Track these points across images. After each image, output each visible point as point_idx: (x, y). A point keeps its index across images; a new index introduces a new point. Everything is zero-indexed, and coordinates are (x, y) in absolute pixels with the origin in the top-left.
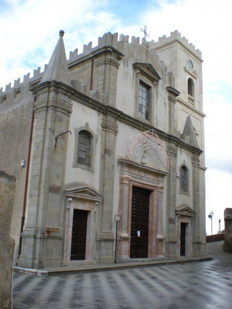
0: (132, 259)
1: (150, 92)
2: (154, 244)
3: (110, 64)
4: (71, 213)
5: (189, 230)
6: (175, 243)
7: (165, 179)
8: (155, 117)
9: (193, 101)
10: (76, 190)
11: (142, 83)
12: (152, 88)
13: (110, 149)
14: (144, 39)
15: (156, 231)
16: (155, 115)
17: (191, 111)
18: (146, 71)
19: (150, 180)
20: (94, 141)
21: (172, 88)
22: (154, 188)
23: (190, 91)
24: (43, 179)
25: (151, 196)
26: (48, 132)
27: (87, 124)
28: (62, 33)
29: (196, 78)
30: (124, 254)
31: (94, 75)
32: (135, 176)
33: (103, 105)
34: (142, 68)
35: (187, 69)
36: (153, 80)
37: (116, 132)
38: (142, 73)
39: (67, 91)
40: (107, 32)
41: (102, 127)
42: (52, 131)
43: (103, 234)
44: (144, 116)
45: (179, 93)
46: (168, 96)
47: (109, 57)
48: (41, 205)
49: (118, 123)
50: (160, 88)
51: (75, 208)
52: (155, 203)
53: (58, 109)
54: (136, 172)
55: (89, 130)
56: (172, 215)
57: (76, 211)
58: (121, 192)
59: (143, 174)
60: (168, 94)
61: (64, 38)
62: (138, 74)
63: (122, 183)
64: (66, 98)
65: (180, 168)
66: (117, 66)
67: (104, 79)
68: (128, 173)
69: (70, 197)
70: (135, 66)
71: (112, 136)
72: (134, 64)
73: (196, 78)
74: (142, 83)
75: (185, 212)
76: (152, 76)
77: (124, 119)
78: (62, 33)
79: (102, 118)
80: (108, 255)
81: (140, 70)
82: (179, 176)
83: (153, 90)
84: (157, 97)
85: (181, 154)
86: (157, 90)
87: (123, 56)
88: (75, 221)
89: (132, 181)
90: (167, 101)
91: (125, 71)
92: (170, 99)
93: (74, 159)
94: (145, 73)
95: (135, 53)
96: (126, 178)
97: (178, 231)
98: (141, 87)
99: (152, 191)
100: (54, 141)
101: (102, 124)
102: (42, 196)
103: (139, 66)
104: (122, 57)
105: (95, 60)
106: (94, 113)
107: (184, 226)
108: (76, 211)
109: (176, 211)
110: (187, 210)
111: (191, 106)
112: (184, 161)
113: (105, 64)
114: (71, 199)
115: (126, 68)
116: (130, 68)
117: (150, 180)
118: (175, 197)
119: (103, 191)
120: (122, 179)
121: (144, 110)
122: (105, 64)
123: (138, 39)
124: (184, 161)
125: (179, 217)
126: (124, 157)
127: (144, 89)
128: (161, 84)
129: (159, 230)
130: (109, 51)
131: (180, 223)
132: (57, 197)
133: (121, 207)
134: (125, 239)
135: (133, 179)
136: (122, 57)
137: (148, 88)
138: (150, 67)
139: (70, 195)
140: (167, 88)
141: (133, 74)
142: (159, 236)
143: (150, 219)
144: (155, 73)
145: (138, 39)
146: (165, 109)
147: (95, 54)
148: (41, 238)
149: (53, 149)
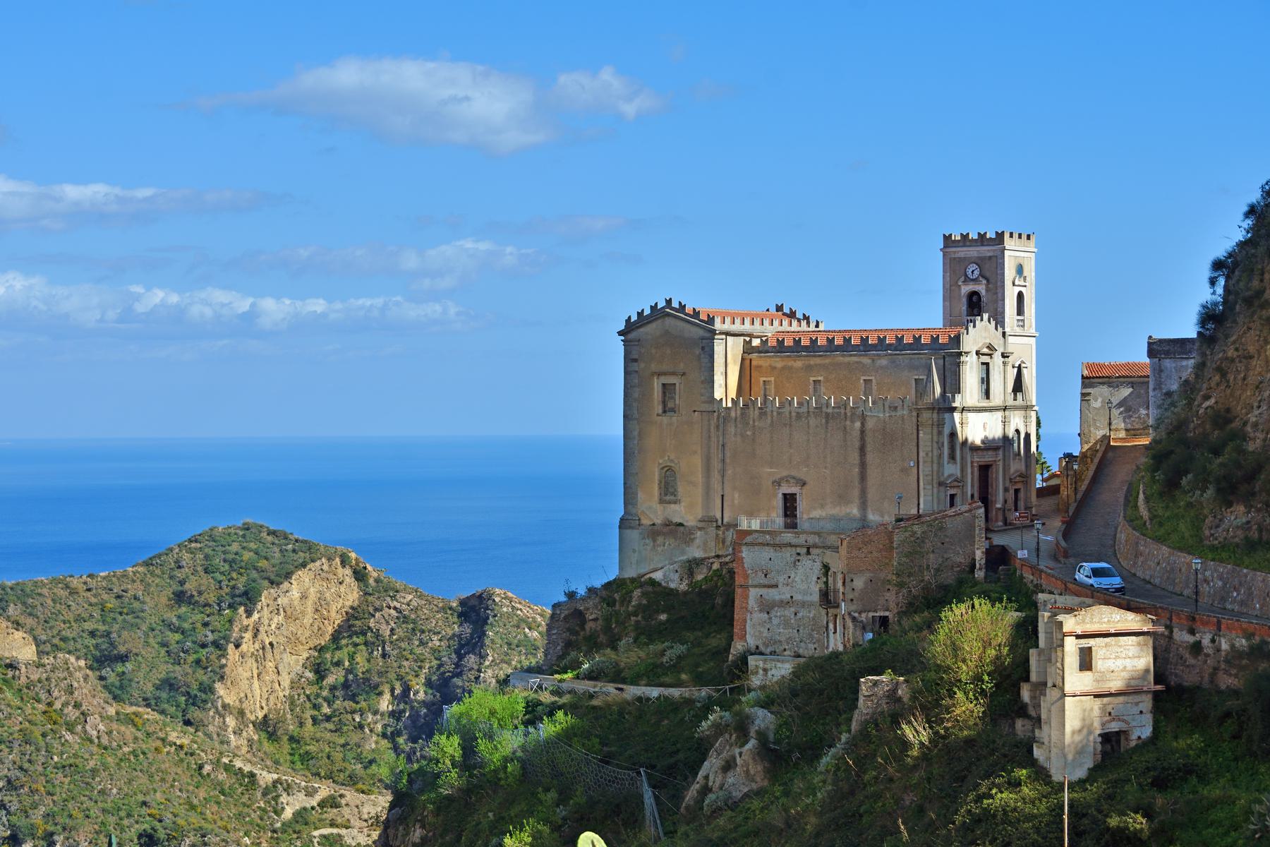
2: (994, 512)
5: (1022, 495)
15: (995, 501)
17: (674, 320)
23: (636, 393)
24: (935, 477)
26: (935, 445)
31: (946, 373)
42: (937, 443)
48: (935, 496)
52: (994, 476)
58: (972, 473)
63: (972, 466)
66: (1147, 457)
102: (935, 490)
107: (1017, 491)
118: (1009, 465)
120: (972, 462)
133: (972, 486)
143: (990, 490)
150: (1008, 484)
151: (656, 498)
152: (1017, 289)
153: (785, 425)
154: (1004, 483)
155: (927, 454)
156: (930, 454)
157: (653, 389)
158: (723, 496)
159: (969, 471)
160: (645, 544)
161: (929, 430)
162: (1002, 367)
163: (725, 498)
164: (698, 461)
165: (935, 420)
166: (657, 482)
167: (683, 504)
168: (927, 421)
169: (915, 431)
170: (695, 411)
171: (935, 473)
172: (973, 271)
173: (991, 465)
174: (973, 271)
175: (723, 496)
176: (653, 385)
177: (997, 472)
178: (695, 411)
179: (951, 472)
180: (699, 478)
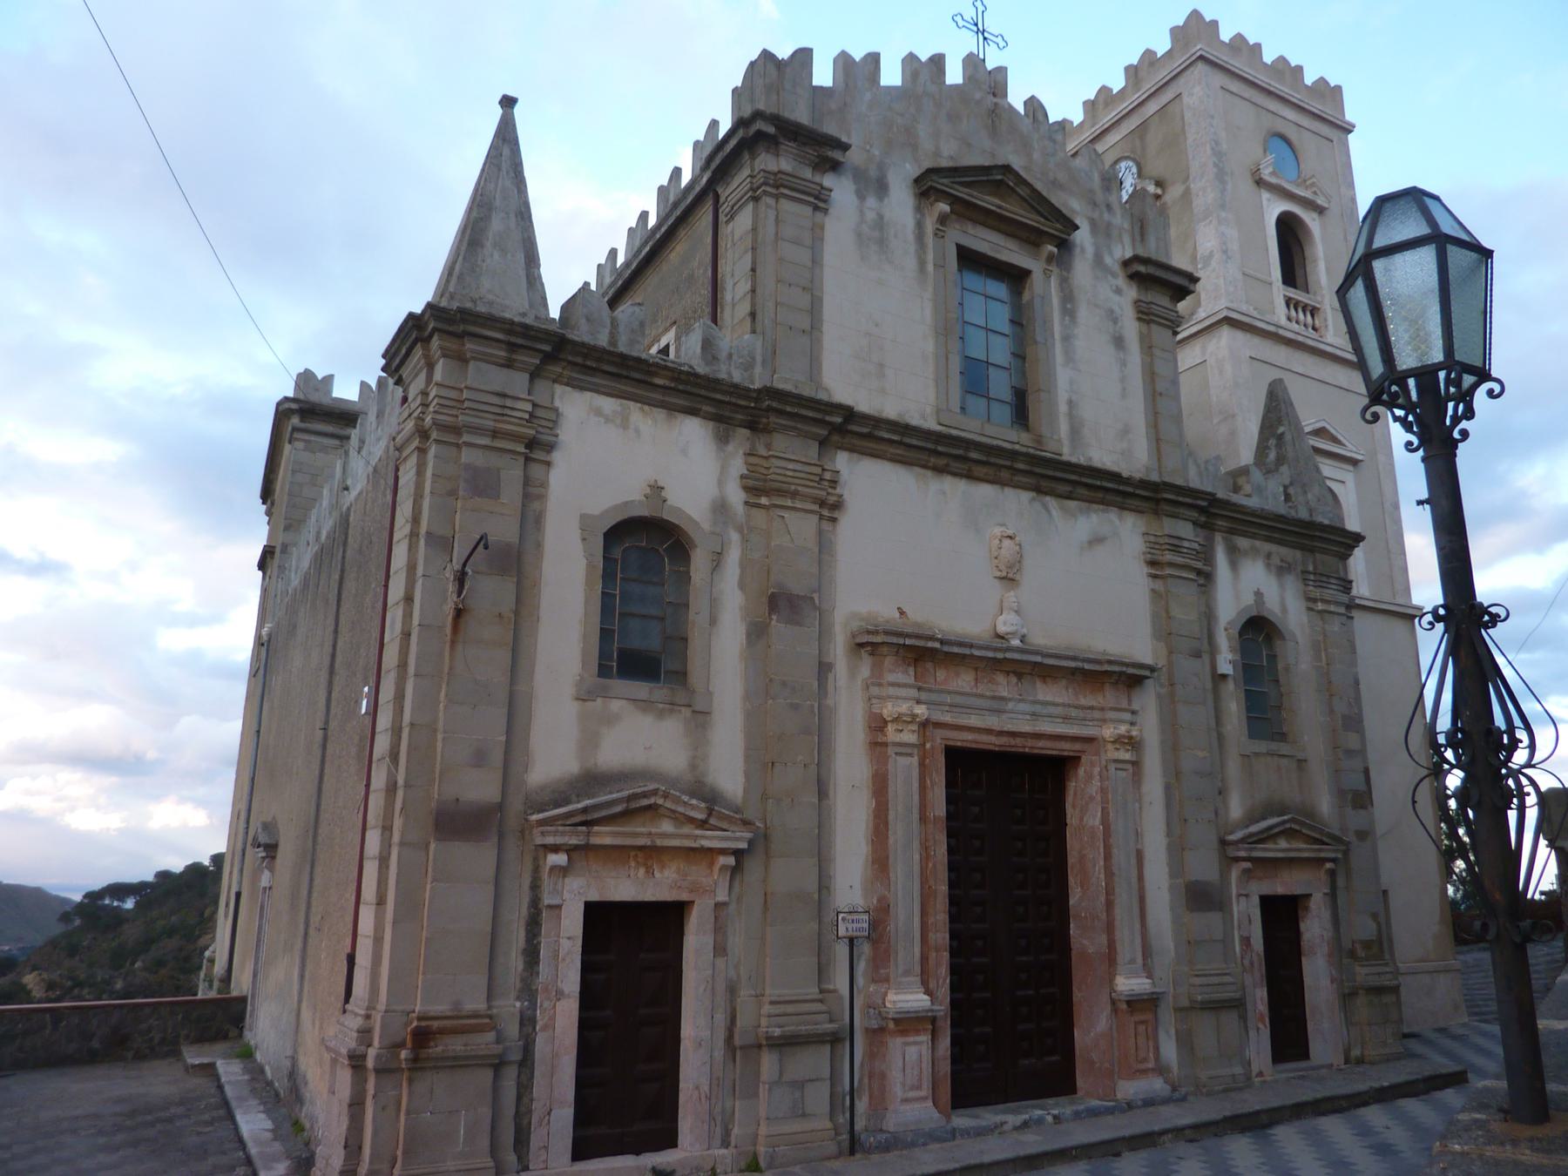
0: (961, 1120)
1: (1026, 296)
3: (777, 197)
4: (572, 924)
6: (1237, 1005)
7: (1148, 701)
8: (1063, 408)
9: (1314, 311)
10: (585, 810)
11: (969, 259)
12: (1037, 276)
13: (797, 587)
14: (973, 63)
15: (1111, 958)
16: (1062, 397)
18: (989, 201)
19: (1051, 710)
20: (699, 562)
21: (1146, 261)
22: (1077, 746)
25: (1072, 786)
27: (656, 489)
28: (508, 102)
29: (1321, 210)
30: (905, 1101)
32: (958, 700)
33: (736, 389)
34: (963, 193)
35: (1266, 174)
36: (1031, 238)
37: (838, 506)
38: (966, 211)
39: (512, 347)
40: (754, 55)
41: (746, 489)
43: (1197, 981)
44: (1003, 413)
45: (1195, 280)
46: (1137, 302)
47: (766, 161)
49: (842, 461)
50: (1082, 269)
51: (594, 896)
53: (466, 438)
54: (964, 681)
55: (1265, 614)
56: (1204, 866)
57: (594, 912)
58: (880, 786)
59: (1004, 686)
60: (1132, 292)
61: (518, 111)
62: (943, 219)
63: (877, 746)
64: (517, 382)
65: (1235, 632)
66: (819, 201)
67: (753, 270)
68: (913, 693)
69: (555, 849)
70: (928, 186)
71: (801, 526)
72: (917, 181)
73: (1321, 210)
74: (969, 259)
75: (1283, 843)
76: (1031, 219)
77: (869, 436)
78: (508, 102)
79: (1143, 529)
80: (804, 1115)
81: (954, 200)
82: (1225, 667)
83: (1044, 286)
84: (1069, 312)
85: (1234, 565)
86: (1064, 282)
87: (845, 147)
88: (955, 944)
89: (938, 725)
90: (1131, 327)
91: (871, 216)
92: (1145, 315)
93: (584, 663)
94: (988, 212)
95: (923, 131)
96: (896, 720)
97: (1246, 941)
98: (974, 281)
99: (1075, 760)
100: (451, 588)
101: (742, 477)
103: (943, 183)
104: (836, 155)
105: (724, 192)
106: (694, 432)
108: (594, 912)
109: (1223, 843)
110: (1290, 834)
111: (1309, 337)
112: (1258, 594)
113: (756, 199)
114: (560, 859)
115: (871, 202)
116: (900, 204)
117: (1051, 710)
119: (764, 797)
120: (877, 725)
121: (1001, 386)
122: (756, 199)
123: (938, 61)
124: (1258, 594)
125: (1246, 871)
126: (885, 612)
127: (999, 289)
128: (1090, 250)
129: (1128, 947)
130: (760, 135)
131: (1256, 900)
132: (477, 858)
133: (880, 862)
134: (907, 1023)
135: (947, 718)
136: (836, 155)
137: (1016, 277)
138: (1000, 178)
139: (550, 840)
140: (1126, 264)
141: (920, 225)
142: (1129, 983)
144: (1038, 202)
145: (938, 61)
146: (1124, 364)
147: (713, 166)
148: (409, 1069)
149: (448, 630)
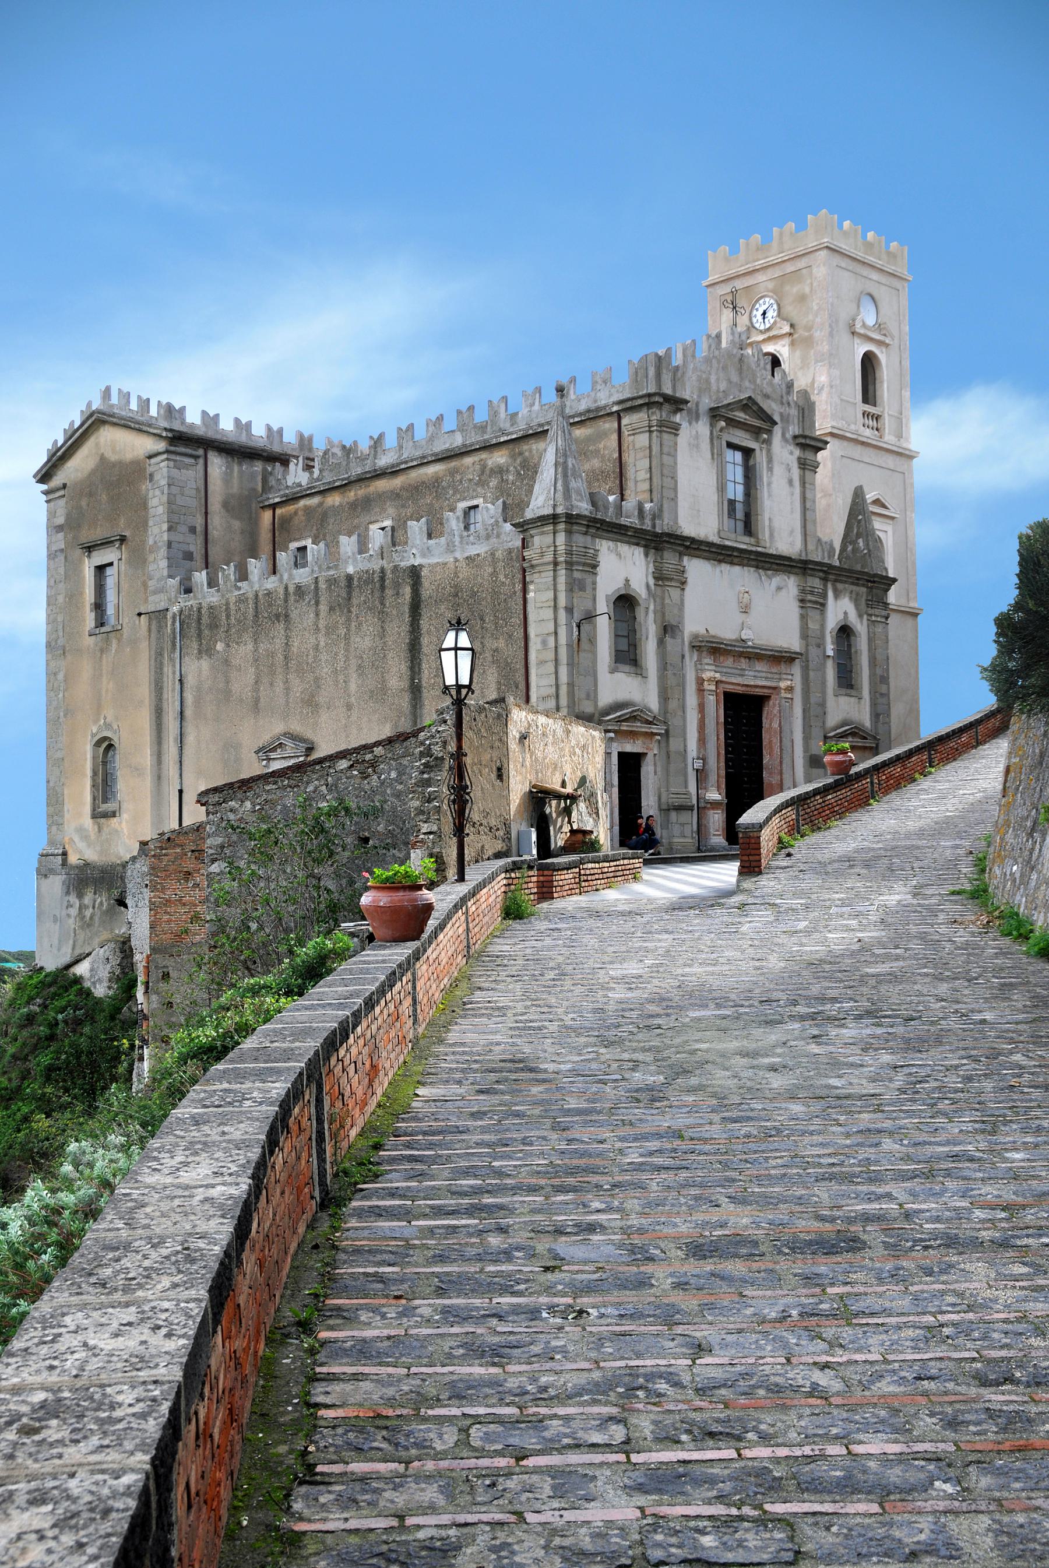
58: (701, 707)
63: (700, 691)
118: (823, 705)
120: (700, 682)
133: (702, 740)
150: (819, 747)
151: (87, 809)
152: (862, 349)
153: (277, 616)
154: (806, 747)
155: (544, 643)
156: (551, 641)
157: (84, 577)
158: (181, 792)
159: (692, 700)
160: (70, 906)
161: (547, 577)
162: (796, 472)
163: (184, 795)
164: (144, 719)
165: (562, 548)
166: (89, 773)
167: (125, 816)
168: (542, 554)
169: (519, 587)
170: (140, 614)
171: (564, 690)
172: (764, 313)
173: (768, 698)
174: (764, 313)
175: (181, 792)
176: (82, 571)
177: (784, 716)
178: (140, 614)
179: (622, 696)
180: (147, 759)
